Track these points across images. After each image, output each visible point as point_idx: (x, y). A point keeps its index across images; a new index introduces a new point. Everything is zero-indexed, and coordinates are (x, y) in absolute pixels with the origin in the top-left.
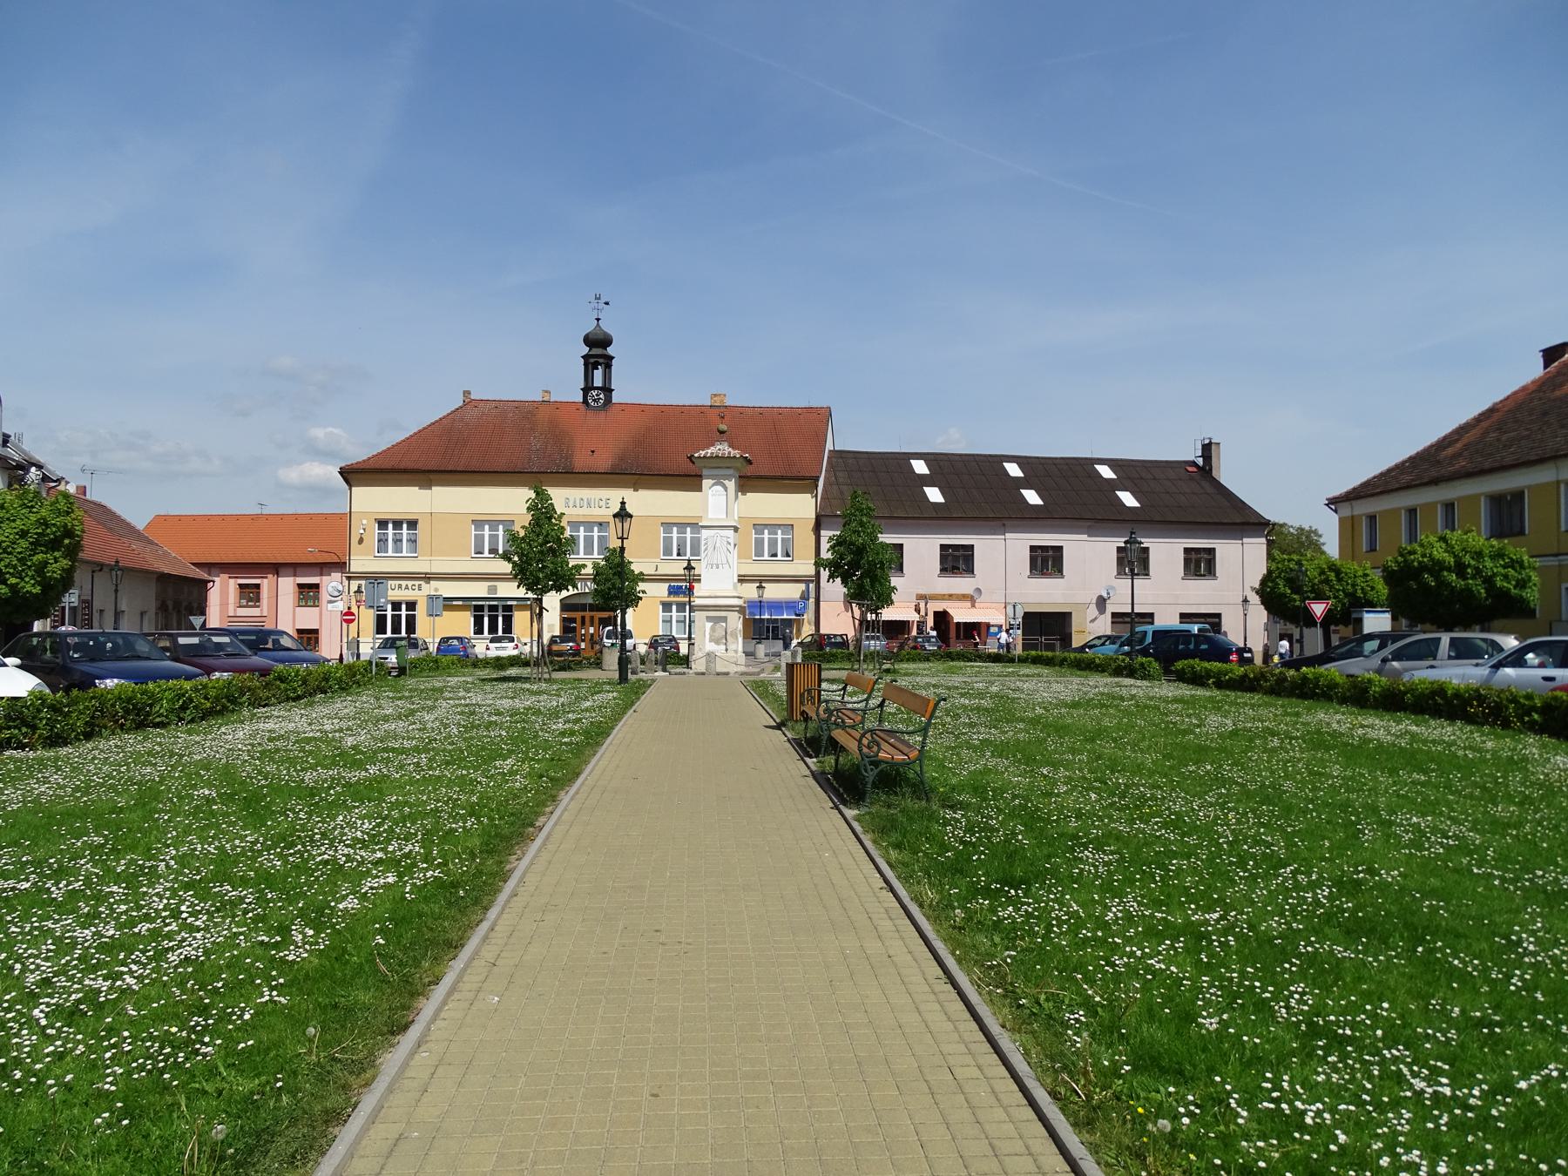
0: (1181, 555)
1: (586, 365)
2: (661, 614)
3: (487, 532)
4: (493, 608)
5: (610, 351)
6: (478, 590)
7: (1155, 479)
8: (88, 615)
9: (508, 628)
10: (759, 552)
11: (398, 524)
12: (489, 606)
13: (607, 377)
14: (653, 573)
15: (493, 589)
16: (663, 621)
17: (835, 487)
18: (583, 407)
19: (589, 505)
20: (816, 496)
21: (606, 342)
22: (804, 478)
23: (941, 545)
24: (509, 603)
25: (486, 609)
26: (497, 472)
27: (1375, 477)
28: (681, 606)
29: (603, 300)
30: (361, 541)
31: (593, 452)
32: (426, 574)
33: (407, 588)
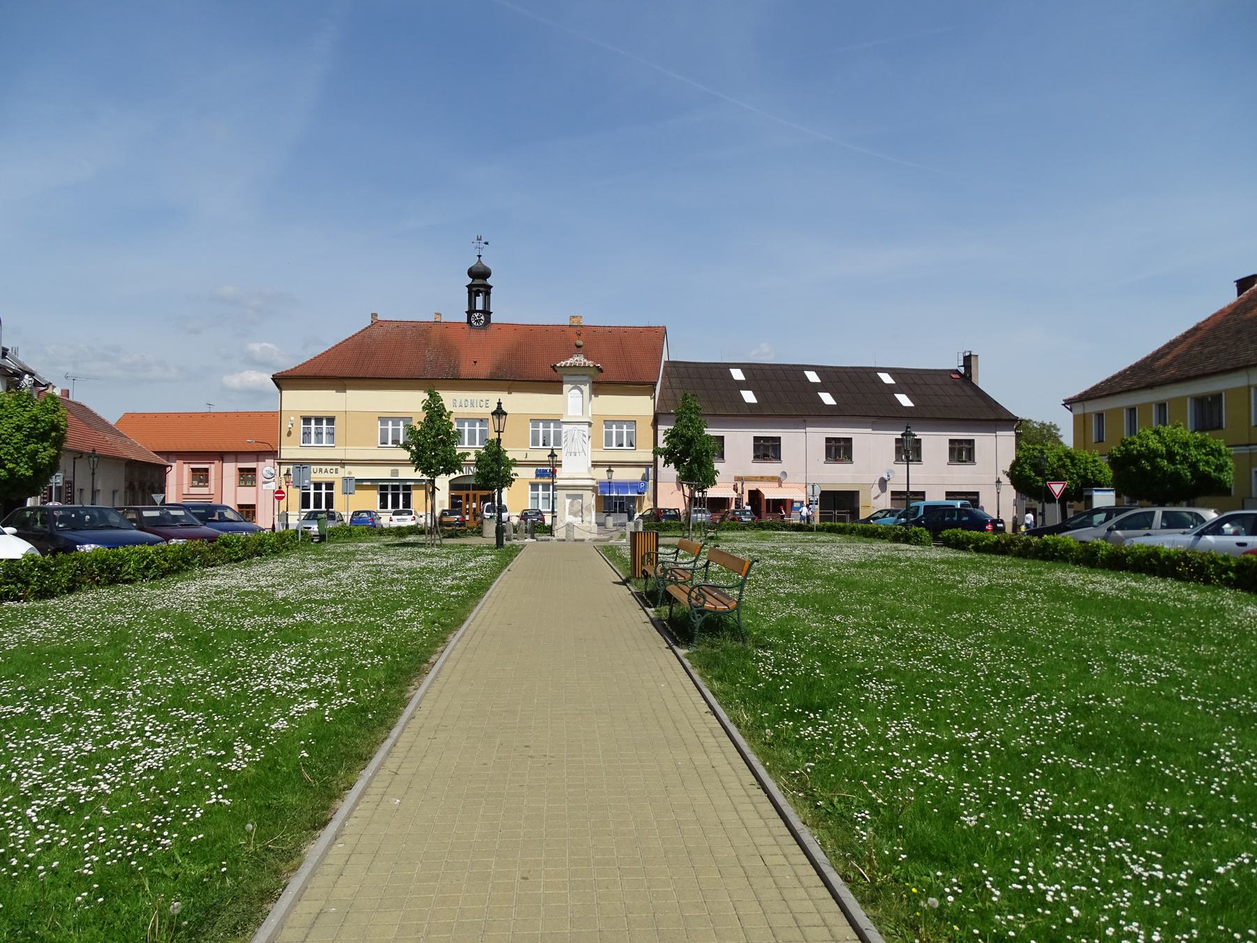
0: (947, 445)
1: (470, 292)
2: (530, 492)
3: (390, 426)
4: (395, 488)
5: (489, 281)
6: (383, 473)
8: (70, 493)
9: (407, 504)
10: (609, 443)
11: (319, 420)
12: (392, 486)
13: (487, 302)
14: (524, 459)
15: (395, 473)
16: (532, 498)
17: (670, 391)
18: (467, 327)
19: (472, 405)
20: (654, 398)
21: (486, 274)
22: (644, 384)
23: (755, 437)
24: (408, 483)
25: (390, 489)
26: (399, 379)
27: (1102, 383)
28: (546, 486)
29: (484, 240)
30: (289, 434)
31: (475, 362)
32: (342, 460)
33: (326, 471)
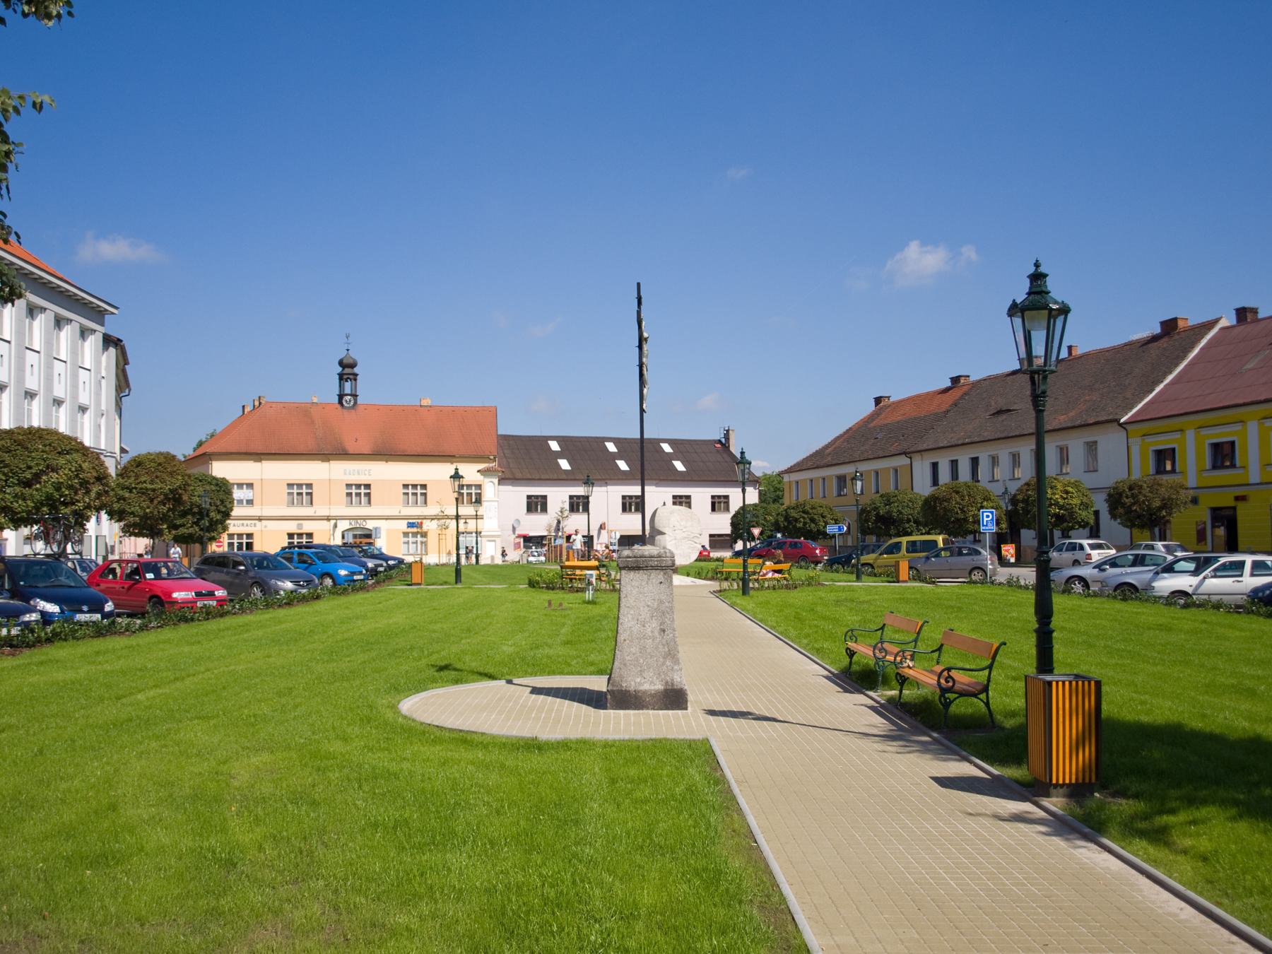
0: (709, 501)
5: (356, 370)
17: (504, 460)
18: (338, 406)
19: (359, 474)
21: (353, 366)
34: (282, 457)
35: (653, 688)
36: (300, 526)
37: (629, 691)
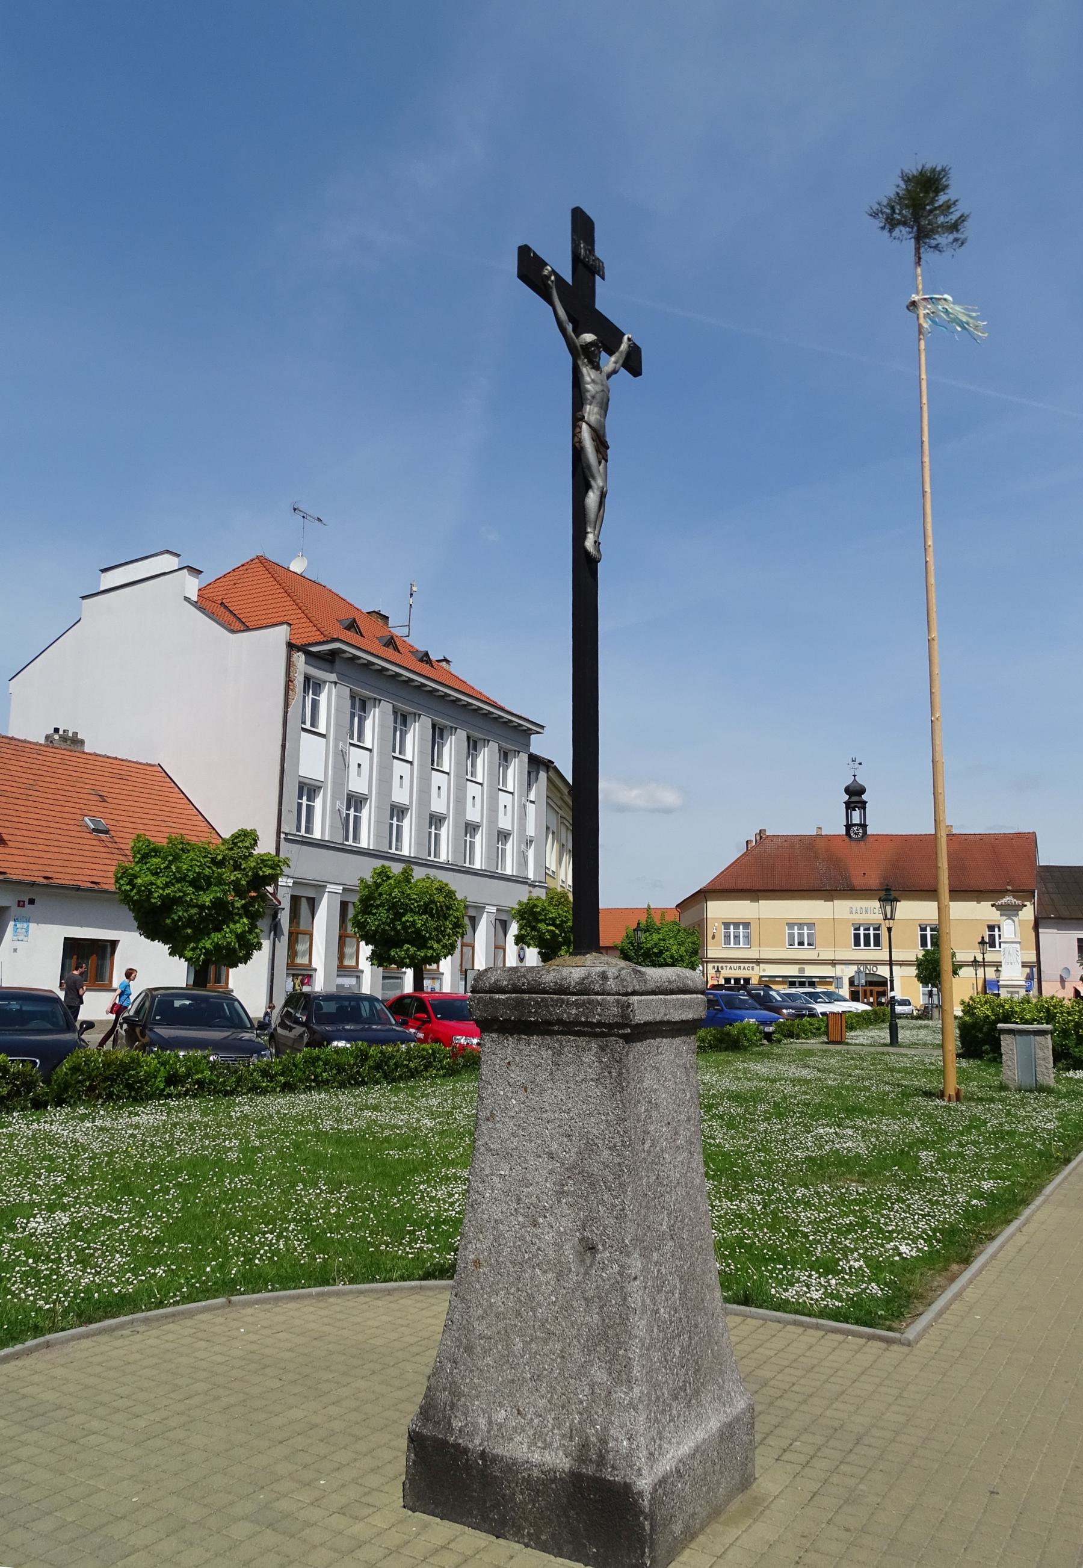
1: (847, 808)
2: (921, 989)
3: (732, 930)
5: (864, 797)
7: (309, 1484)
11: (736, 925)
15: (802, 970)
17: (1046, 895)
18: (847, 839)
19: (867, 912)
21: (862, 791)
24: (814, 980)
29: (858, 761)
30: (713, 937)
33: (744, 968)
34: (790, 893)
35: (536, 1457)
36: (802, 970)
37: (465, 1451)
